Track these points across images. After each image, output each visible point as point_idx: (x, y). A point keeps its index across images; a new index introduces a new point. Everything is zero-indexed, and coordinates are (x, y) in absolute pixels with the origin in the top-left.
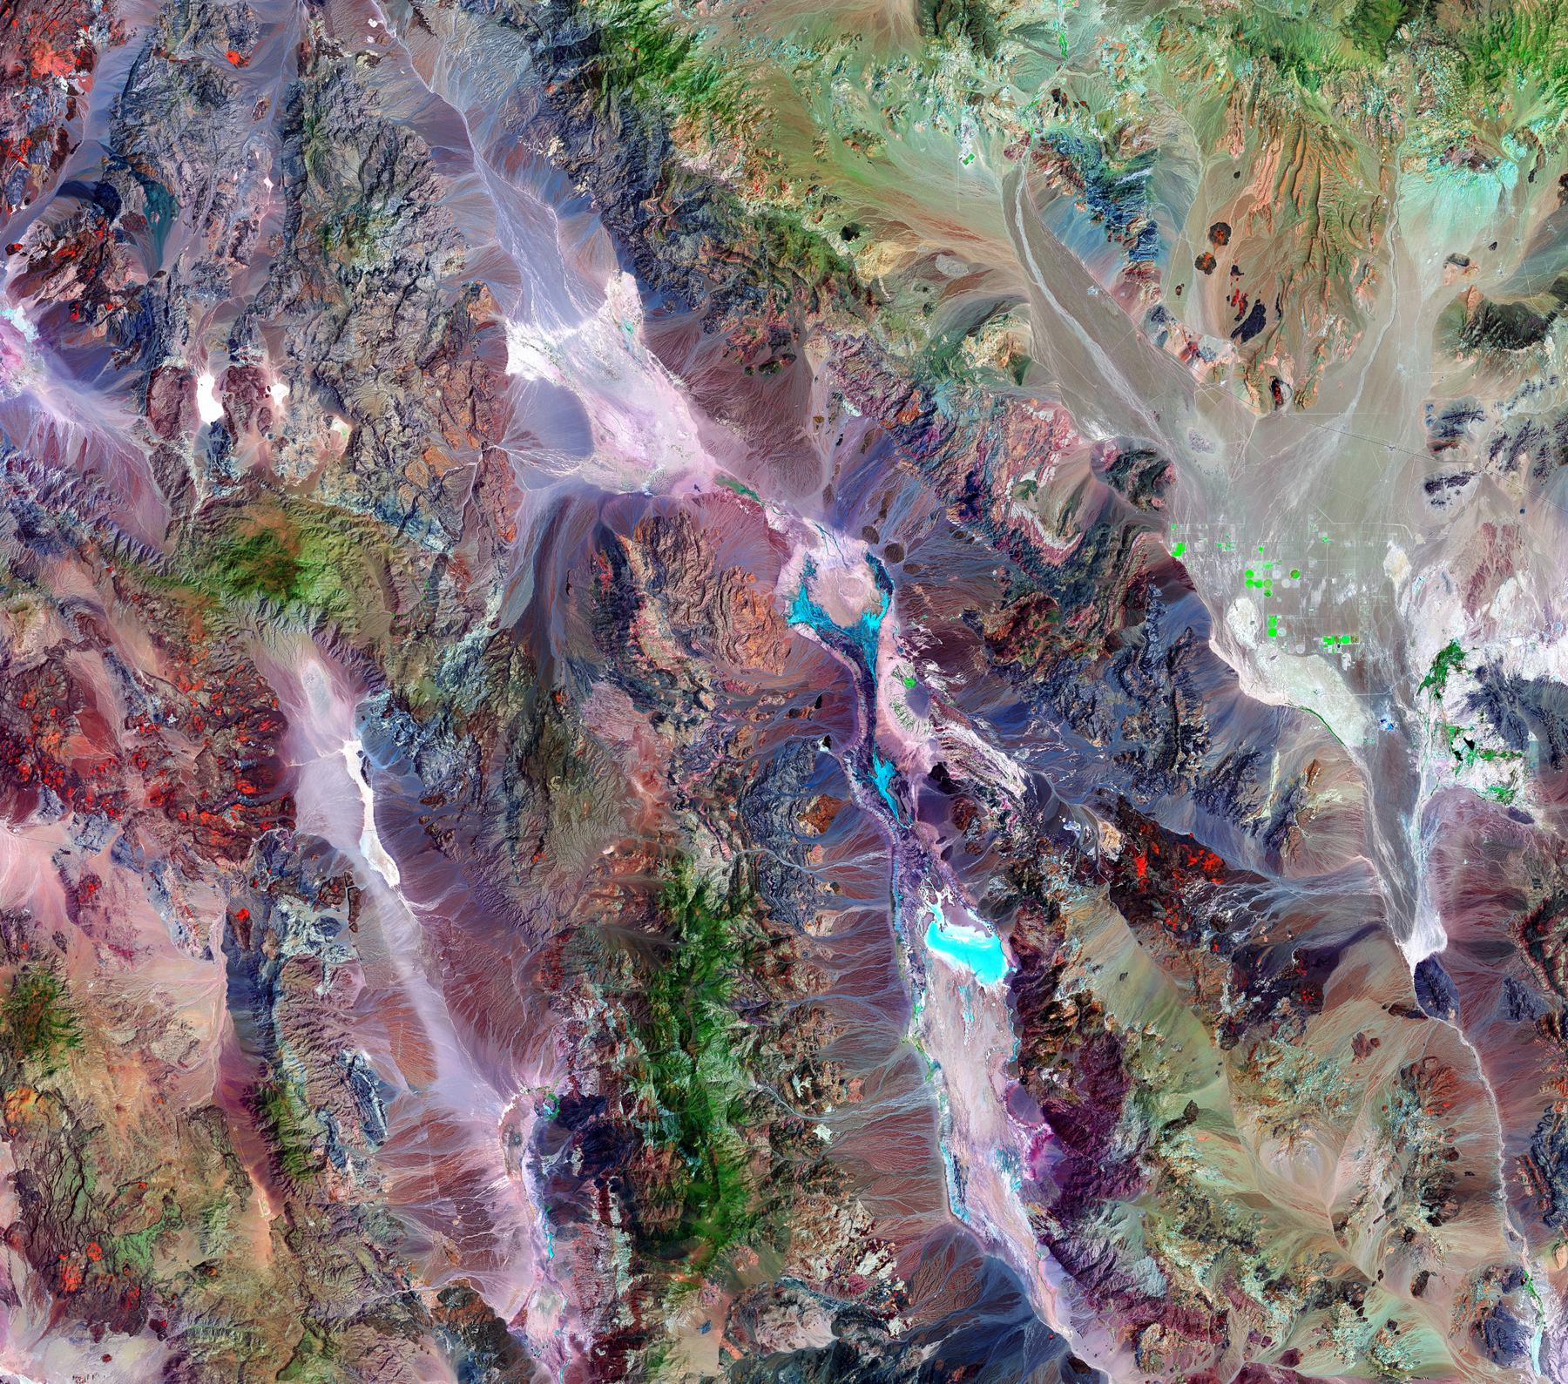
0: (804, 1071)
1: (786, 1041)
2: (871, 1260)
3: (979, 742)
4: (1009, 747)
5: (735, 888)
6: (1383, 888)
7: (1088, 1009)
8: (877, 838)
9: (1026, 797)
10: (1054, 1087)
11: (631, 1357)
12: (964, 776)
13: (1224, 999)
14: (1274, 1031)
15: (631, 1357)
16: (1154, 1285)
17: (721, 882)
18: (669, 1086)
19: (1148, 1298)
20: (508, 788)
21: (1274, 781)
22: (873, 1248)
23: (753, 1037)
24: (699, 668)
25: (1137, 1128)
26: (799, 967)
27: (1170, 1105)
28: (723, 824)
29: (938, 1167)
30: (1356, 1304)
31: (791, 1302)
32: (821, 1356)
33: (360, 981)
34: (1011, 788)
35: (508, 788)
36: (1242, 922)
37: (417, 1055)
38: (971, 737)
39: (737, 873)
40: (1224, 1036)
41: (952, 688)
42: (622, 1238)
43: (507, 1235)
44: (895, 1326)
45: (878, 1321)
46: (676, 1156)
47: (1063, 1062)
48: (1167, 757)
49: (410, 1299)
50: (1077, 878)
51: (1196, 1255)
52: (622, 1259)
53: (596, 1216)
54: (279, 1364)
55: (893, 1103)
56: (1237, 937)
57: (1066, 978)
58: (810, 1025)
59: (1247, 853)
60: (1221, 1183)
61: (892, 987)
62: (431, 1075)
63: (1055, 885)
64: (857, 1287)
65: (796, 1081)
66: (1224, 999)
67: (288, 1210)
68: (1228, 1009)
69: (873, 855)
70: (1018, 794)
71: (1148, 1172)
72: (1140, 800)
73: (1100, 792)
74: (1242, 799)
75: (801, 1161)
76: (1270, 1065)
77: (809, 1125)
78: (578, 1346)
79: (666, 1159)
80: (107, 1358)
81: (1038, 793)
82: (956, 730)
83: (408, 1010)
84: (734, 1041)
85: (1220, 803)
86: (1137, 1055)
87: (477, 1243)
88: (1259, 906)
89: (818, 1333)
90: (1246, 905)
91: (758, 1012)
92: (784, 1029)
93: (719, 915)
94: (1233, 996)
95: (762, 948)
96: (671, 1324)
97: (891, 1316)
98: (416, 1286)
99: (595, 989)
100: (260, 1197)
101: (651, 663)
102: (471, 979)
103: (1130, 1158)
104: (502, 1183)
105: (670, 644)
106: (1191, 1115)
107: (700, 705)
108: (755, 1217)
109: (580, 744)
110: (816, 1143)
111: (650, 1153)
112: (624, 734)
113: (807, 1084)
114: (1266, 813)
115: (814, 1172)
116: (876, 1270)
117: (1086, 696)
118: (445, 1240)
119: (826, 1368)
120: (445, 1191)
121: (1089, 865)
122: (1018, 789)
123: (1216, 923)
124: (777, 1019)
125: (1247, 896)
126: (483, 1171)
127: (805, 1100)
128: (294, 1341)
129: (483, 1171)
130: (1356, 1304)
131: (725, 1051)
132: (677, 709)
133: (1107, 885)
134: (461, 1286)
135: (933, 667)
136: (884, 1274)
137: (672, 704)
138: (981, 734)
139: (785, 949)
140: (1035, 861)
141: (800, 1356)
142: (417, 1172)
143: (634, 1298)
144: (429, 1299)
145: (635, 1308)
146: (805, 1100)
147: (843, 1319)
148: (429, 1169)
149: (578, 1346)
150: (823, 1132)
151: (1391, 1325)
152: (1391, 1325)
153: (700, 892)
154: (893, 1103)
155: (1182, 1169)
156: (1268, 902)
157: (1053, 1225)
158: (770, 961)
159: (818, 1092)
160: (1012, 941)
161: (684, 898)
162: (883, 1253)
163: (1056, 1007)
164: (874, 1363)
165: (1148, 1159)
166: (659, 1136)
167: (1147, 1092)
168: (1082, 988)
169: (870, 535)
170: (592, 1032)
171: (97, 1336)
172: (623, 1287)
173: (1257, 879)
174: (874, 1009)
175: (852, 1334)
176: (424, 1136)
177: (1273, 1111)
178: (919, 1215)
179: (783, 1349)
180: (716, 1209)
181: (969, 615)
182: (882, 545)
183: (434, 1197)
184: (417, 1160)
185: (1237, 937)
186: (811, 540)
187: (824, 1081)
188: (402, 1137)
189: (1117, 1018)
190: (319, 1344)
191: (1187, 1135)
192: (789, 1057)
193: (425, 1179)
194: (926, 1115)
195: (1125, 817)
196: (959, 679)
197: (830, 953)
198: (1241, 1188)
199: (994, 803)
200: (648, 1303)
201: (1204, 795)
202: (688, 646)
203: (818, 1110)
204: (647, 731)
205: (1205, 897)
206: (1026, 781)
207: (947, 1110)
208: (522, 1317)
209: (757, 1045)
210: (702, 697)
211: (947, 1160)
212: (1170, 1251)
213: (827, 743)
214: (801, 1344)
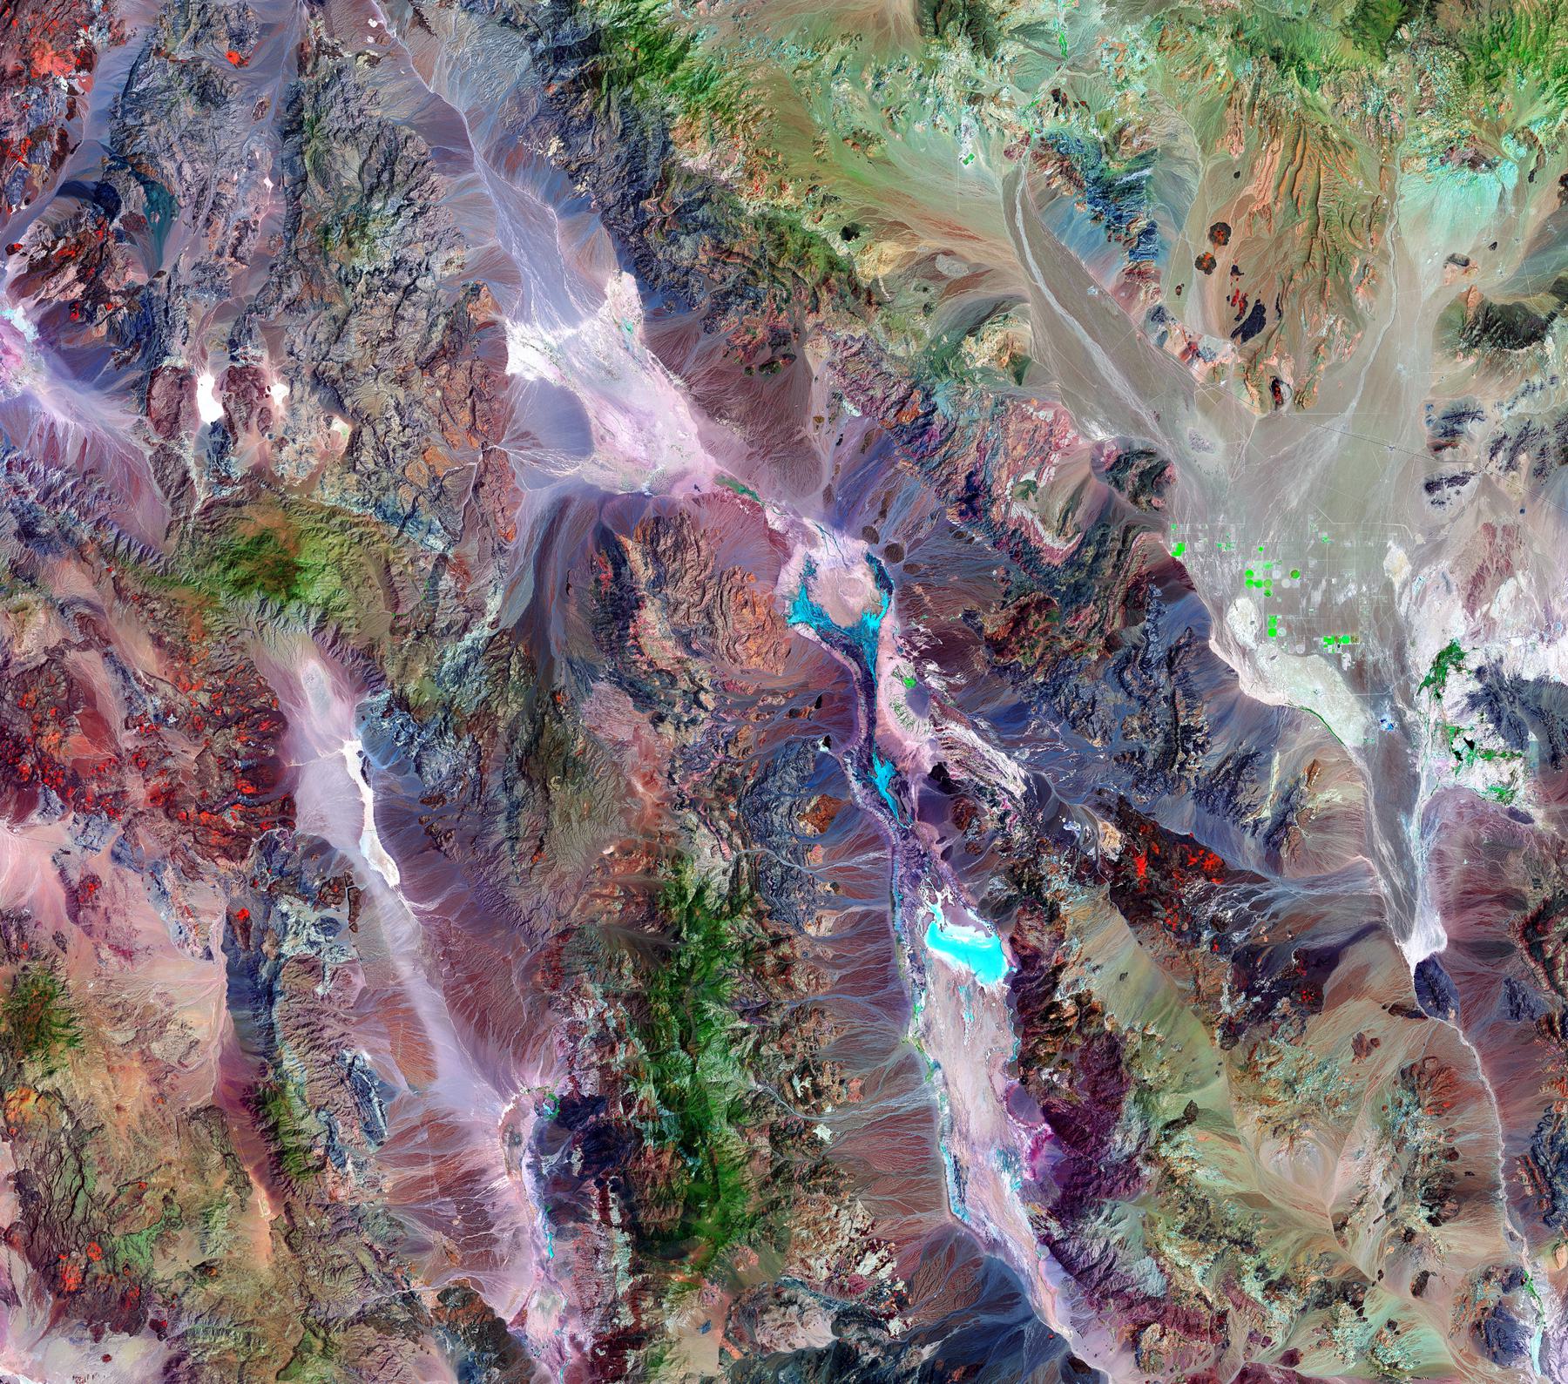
0: (804, 1071)
1: (786, 1041)
2: (871, 1260)
3: (979, 742)
4: (1009, 747)
5: (735, 888)
6: (1384, 888)
7: (1088, 1009)
8: (876, 838)
9: (1026, 797)
10: (1054, 1087)
11: (631, 1357)
12: (964, 776)
13: (1224, 999)
14: (1274, 1031)
15: (631, 1357)
16: (1154, 1285)
17: (721, 882)
18: (669, 1085)
19: (1147, 1298)
20: (508, 788)
21: (1274, 781)
22: (873, 1248)
23: (753, 1037)
24: (699, 668)
25: (1137, 1128)
26: (799, 967)
27: (1170, 1105)
28: (723, 824)
29: (938, 1167)
30: (1356, 1304)
31: (791, 1302)
32: (821, 1356)
33: (360, 981)
34: (1011, 788)
35: (508, 788)
36: (1242, 922)
37: (417, 1055)
38: (971, 737)
39: (736, 873)
40: (1224, 1036)
41: (952, 688)
42: (622, 1238)
43: (507, 1235)
44: (895, 1326)
45: (878, 1321)
46: (676, 1156)
47: (1063, 1062)
48: (1167, 757)
49: (410, 1299)
50: (1077, 878)
51: (1196, 1255)
52: (622, 1259)
53: (596, 1216)
54: (279, 1364)
55: (893, 1103)
56: (1237, 937)
57: (1066, 978)
58: (810, 1025)
59: (1247, 853)
60: (1221, 1183)
61: (892, 987)
62: (431, 1075)
63: (1055, 885)
64: (857, 1287)
65: (796, 1081)
66: (1224, 999)
67: (288, 1210)
68: (1228, 1009)
69: (873, 855)
70: (1018, 794)
71: (1148, 1172)
72: (1140, 800)
73: (1100, 792)
74: (1242, 799)
75: (801, 1161)
76: (1270, 1065)
77: (809, 1125)
78: (578, 1346)
79: (666, 1159)
80: (107, 1358)
81: (1038, 793)
82: (956, 730)
83: (408, 1010)
84: (734, 1041)
85: (1220, 803)
86: (1137, 1055)
87: (477, 1243)
88: (1259, 906)
89: (818, 1333)
90: (1246, 905)
91: (758, 1012)
92: (784, 1029)
93: (719, 915)
94: (1233, 996)
95: (762, 948)
96: (671, 1324)
97: (891, 1316)
98: (416, 1286)
99: (595, 989)
100: (260, 1197)
101: (651, 663)
102: (471, 979)
103: (1130, 1158)
104: (502, 1183)
105: (670, 644)
106: (1191, 1115)
107: (700, 705)
108: (755, 1217)
109: (580, 744)
110: (816, 1143)
111: (650, 1153)
112: (624, 734)
113: (807, 1084)
114: (1266, 813)
115: (814, 1172)
116: (876, 1269)
117: (1086, 696)
118: (445, 1240)
119: (826, 1368)
120: (445, 1191)
121: (1089, 865)
122: (1018, 789)
123: (1216, 923)
124: (777, 1019)
125: (1247, 896)
126: (483, 1171)
127: (805, 1100)
128: (294, 1341)
129: (483, 1171)
130: (1356, 1304)
131: (725, 1051)
132: (677, 709)
133: (1107, 885)
134: (461, 1286)
135: (933, 667)
136: (884, 1274)
137: (672, 704)
138: (982, 734)
139: (785, 949)
140: (1035, 861)
141: (800, 1356)
142: (417, 1172)
143: (634, 1298)
144: (429, 1299)
145: (635, 1308)
146: (805, 1100)
147: (843, 1319)
148: (429, 1169)
149: (578, 1346)
150: (823, 1132)
151: (1391, 1325)
152: (1391, 1325)
153: (700, 892)
154: (893, 1103)
155: (1182, 1169)
156: (1268, 902)
157: (1053, 1224)
158: (770, 961)
159: (818, 1092)
160: (1013, 941)
161: (684, 898)
162: (883, 1253)
163: (1056, 1007)
164: (874, 1363)
165: (1148, 1159)
166: (659, 1136)
167: (1147, 1092)
168: (1082, 988)
169: (870, 535)
170: (592, 1032)
171: (97, 1336)
172: (623, 1287)
173: (1257, 879)
174: (874, 1009)
175: (852, 1334)
176: (424, 1136)
177: (1273, 1111)
178: (918, 1215)
179: (783, 1349)
180: (716, 1209)
181: (969, 615)
182: (882, 545)
183: (434, 1197)
184: (418, 1160)
185: (1237, 937)
186: (811, 540)
187: (825, 1081)
188: (401, 1137)
189: (1117, 1018)
190: (319, 1344)
191: (1187, 1134)
192: (789, 1057)
193: (425, 1179)
194: (926, 1115)
195: (1125, 817)
196: (959, 679)
197: (830, 953)
198: (1241, 1188)
199: (994, 803)
200: (648, 1303)
201: (1204, 795)
202: (688, 646)
203: (818, 1110)
204: (647, 731)
205: (1206, 897)
206: (1026, 781)
207: (947, 1110)
208: (522, 1317)
209: (757, 1046)
210: (703, 697)
211: (947, 1160)
212: (1170, 1251)
213: (827, 743)
214: (801, 1344)
